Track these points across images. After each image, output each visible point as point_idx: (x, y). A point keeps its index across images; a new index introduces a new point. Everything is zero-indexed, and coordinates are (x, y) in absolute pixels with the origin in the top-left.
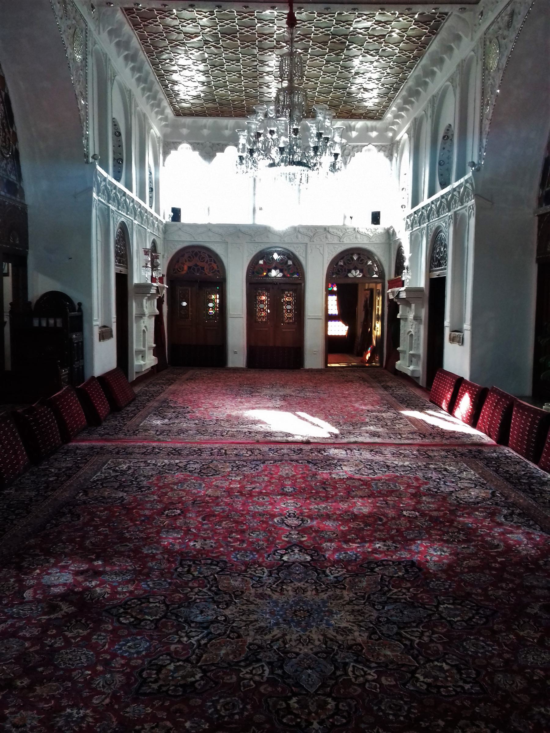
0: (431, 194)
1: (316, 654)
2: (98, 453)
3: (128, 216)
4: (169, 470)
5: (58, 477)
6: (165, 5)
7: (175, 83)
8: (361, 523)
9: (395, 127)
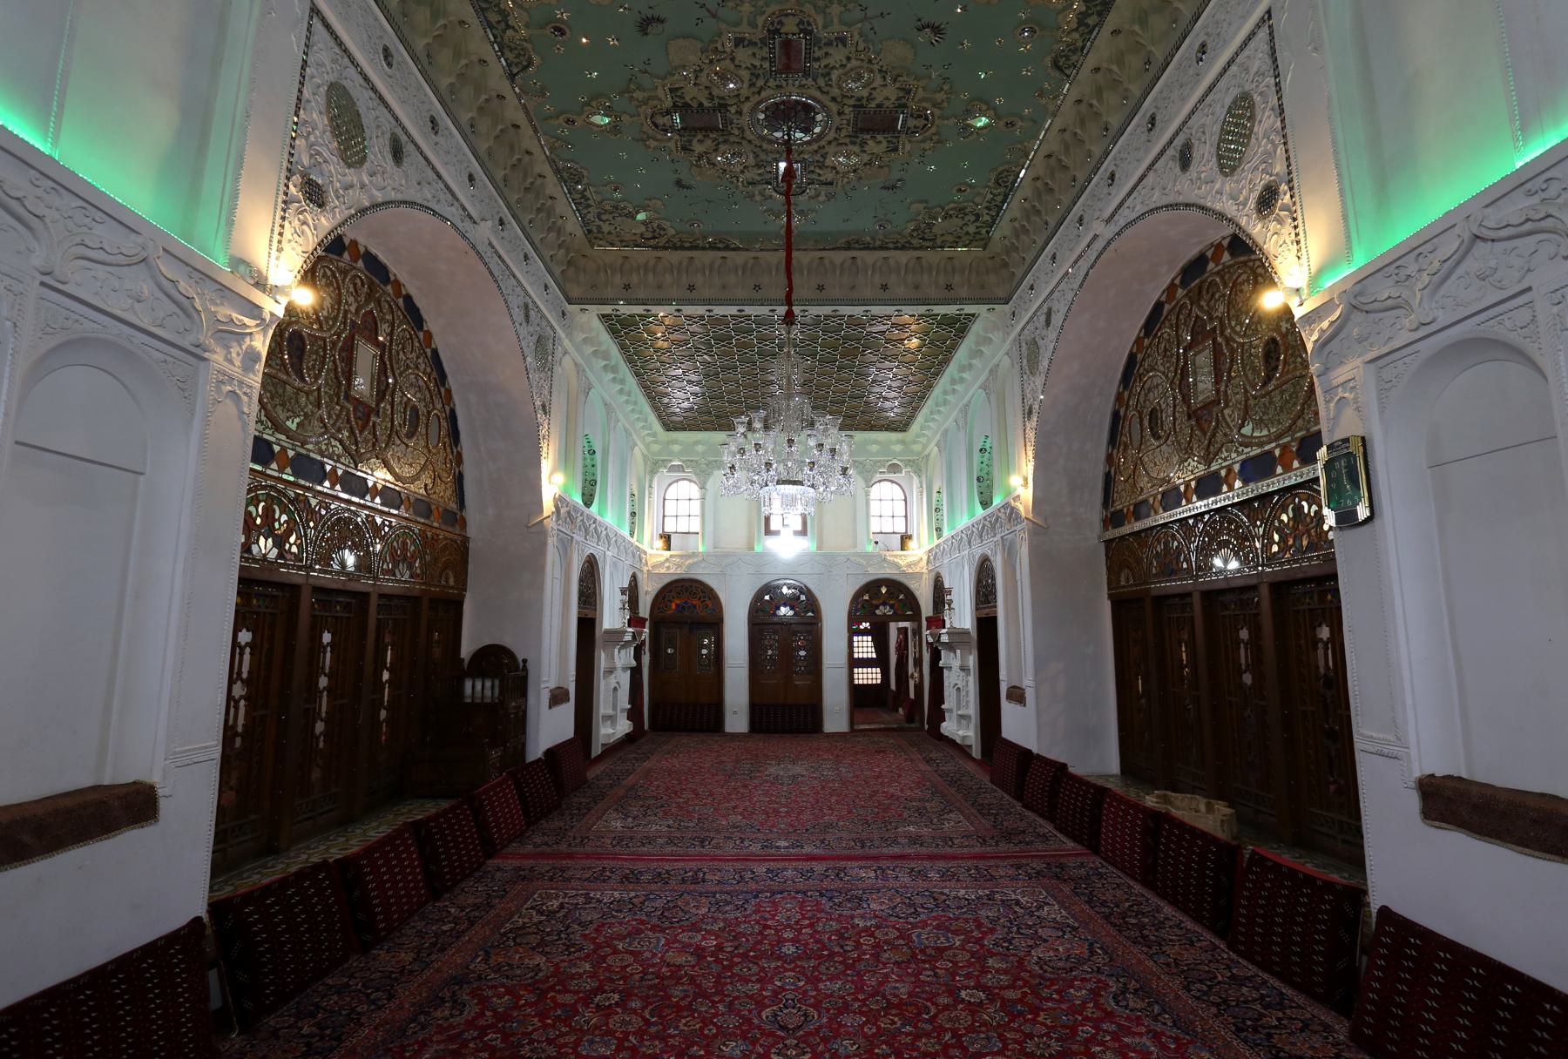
4: (617, 912)
5: (456, 924)
6: (648, 311)
8: (896, 1019)
9: (923, 440)
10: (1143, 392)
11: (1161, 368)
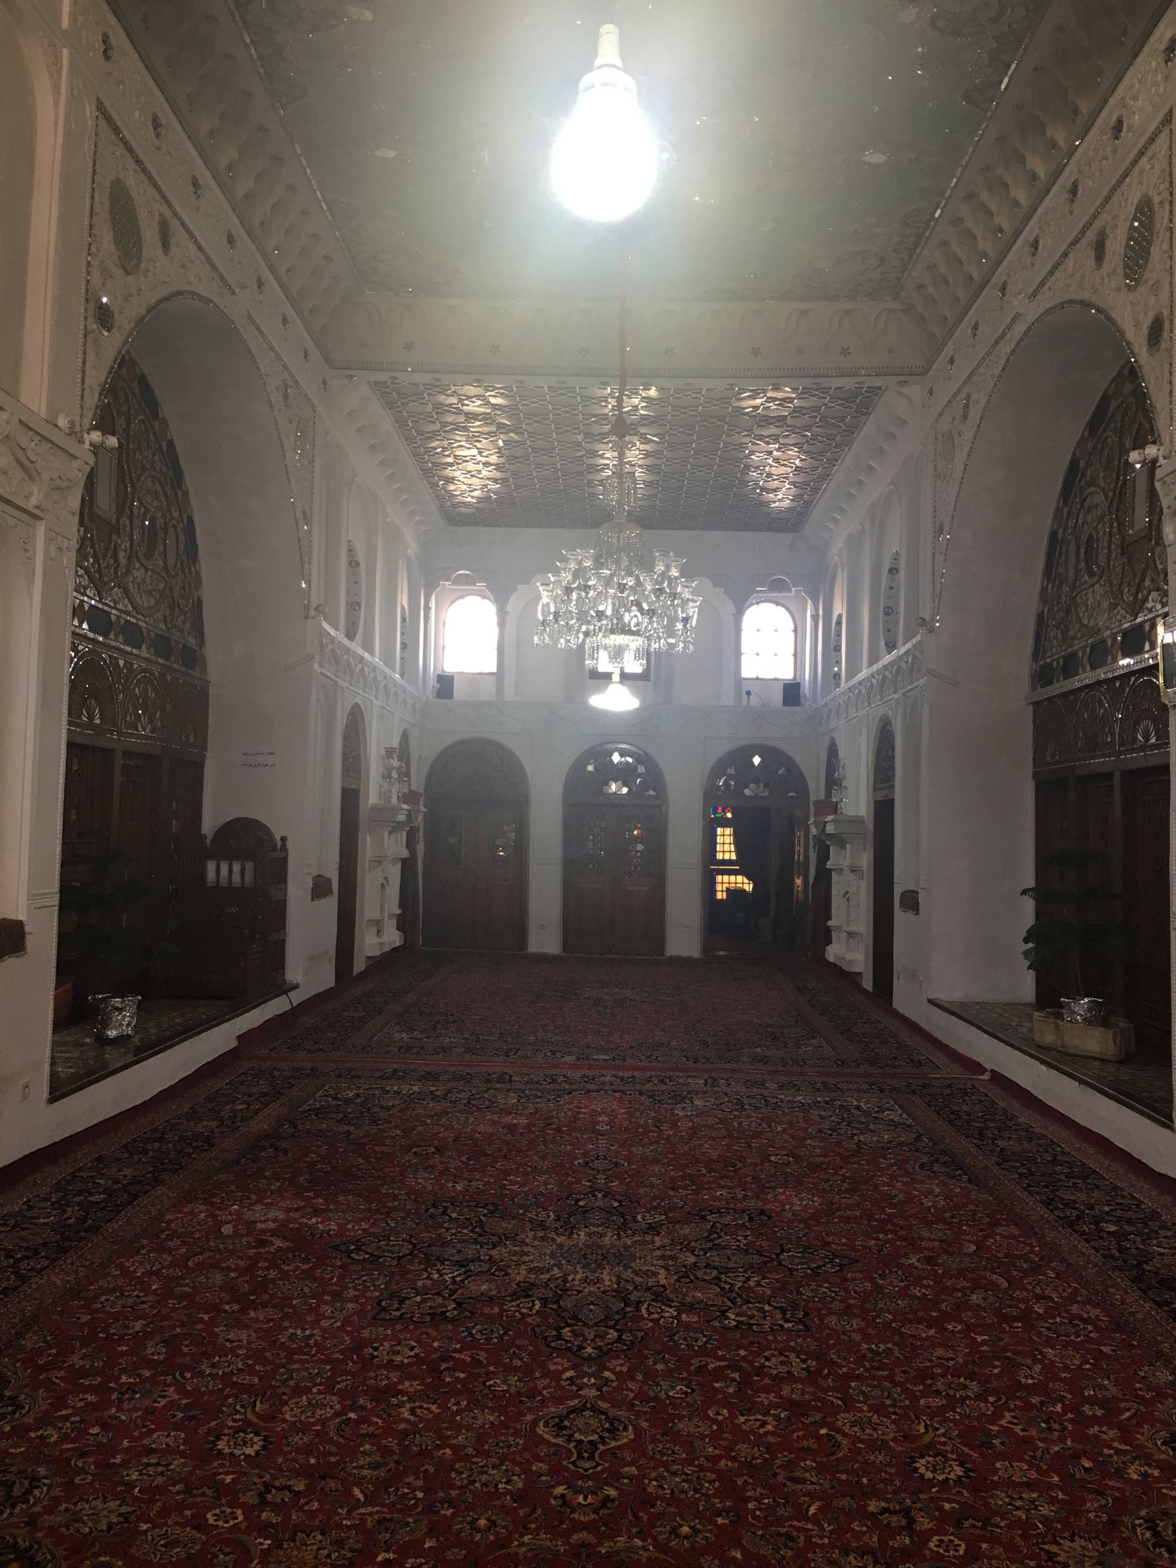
0: (873, 660)
1: (604, 1292)
2: (307, 1075)
3: (365, 695)
5: (249, 1105)
6: (437, 380)
7: (451, 480)
10: (1082, 512)
11: (1102, 484)
